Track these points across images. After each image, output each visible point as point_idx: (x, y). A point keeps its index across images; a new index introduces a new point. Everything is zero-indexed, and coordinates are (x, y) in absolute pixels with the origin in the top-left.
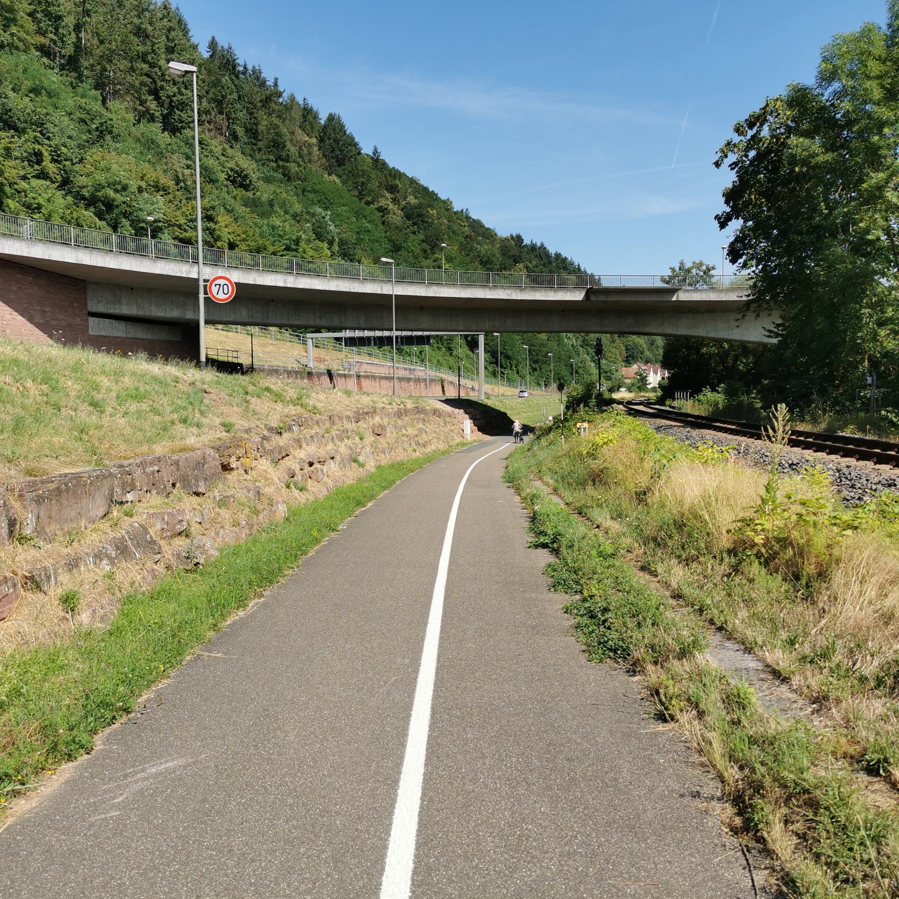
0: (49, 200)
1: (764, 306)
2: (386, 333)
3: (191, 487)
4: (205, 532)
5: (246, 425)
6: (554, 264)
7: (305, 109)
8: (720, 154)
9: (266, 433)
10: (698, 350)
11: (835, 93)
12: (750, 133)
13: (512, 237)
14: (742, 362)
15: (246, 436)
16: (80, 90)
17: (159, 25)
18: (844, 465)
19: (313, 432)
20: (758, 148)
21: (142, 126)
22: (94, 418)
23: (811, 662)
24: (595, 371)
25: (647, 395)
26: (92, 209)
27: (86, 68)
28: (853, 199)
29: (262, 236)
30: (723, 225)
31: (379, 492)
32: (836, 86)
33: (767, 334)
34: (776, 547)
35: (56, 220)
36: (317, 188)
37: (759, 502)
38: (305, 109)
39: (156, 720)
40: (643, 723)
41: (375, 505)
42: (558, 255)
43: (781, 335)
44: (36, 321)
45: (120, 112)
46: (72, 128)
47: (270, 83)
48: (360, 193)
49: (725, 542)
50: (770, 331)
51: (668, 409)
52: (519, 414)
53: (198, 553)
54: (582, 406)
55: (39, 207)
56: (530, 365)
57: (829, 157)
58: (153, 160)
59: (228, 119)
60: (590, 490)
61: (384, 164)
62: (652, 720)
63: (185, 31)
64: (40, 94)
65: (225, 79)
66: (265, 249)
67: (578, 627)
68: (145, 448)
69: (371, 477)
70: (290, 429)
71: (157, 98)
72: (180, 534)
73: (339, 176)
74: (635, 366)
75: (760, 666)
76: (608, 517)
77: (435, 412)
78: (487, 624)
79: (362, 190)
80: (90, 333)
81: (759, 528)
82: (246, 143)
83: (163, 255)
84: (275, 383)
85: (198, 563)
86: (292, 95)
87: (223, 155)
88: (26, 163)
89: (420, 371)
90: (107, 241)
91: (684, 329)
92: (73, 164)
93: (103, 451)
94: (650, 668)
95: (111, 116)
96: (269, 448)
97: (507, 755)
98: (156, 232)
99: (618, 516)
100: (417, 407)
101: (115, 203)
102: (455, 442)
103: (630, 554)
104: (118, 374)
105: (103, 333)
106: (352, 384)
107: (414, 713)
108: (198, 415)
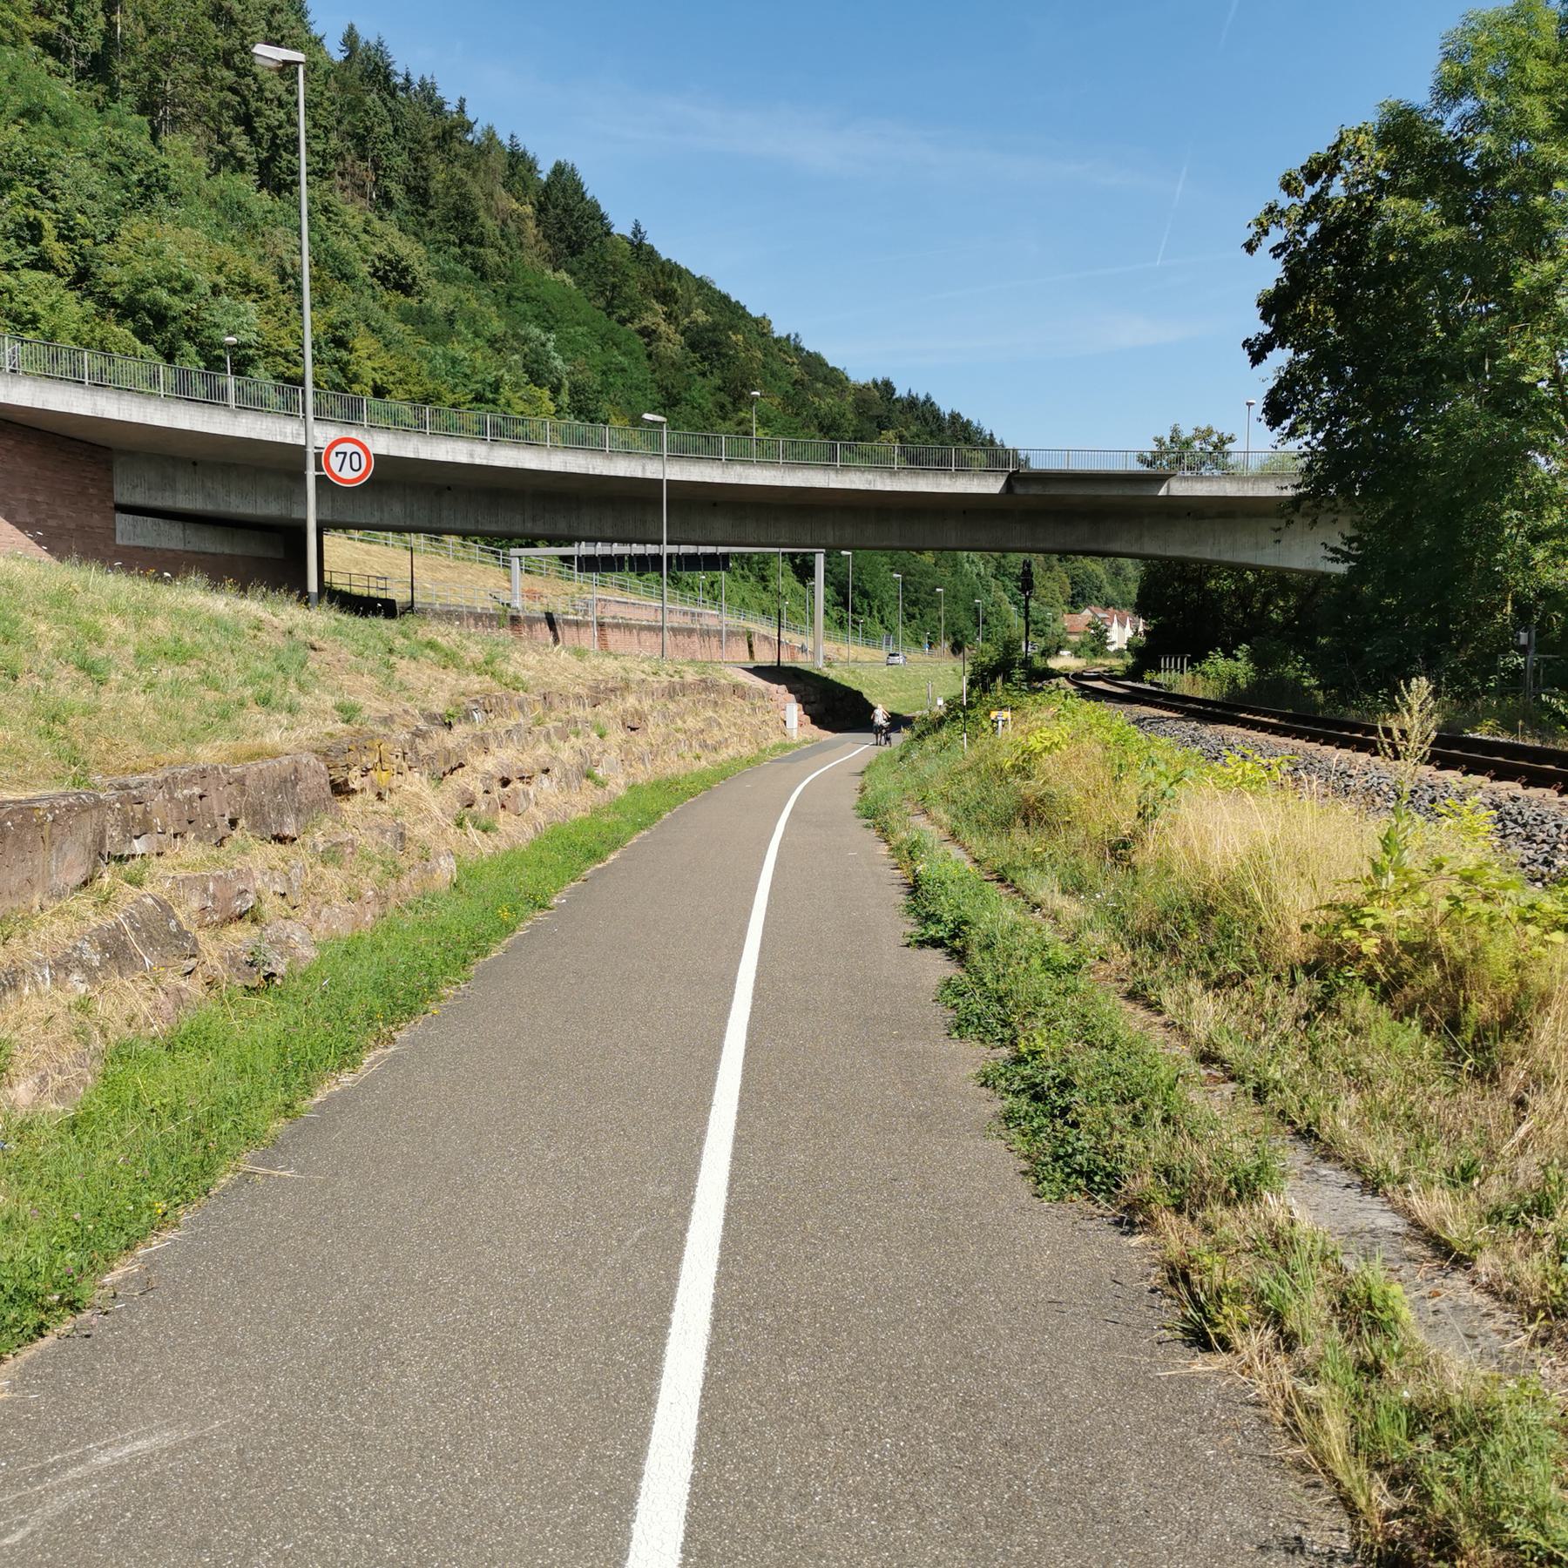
0: (52, 307)
1: (1326, 505)
2: (651, 549)
3: (268, 826)
4: (292, 913)
5: (386, 709)
6: (949, 432)
7: (512, 154)
8: (1254, 229)
9: (422, 724)
10: (1199, 582)
11: (1463, 118)
12: (1310, 191)
13: (875, 383)
14: (1277, 607)
15: (382, 730)
16: (112, 115)
18: (1503, 794)
19: (511, 723)
20: (1324, 219)
21: (221, 180)
22: (84, 692)
23: (1514, 1222)
24: (1017, 622)
25: (1107, 662)
27: (124, 77)
28: (1490, 313)
29: (433, 374)
30: (1257, 358)
31: (630, 836)
32: (1468, 105)
33: (1331, 555)
34: (1407, 962)
35: (65, 341)
36: (533, 292)
37: (1368, 870)
38: (512, 154)
39: (132, 1330)
40: (1159, 1352)
42: (955, 417)
43: (1354, 558)
44: (19, 519)
45: (182, 153)
46: (95, 181)
47: (451, 107)
48: (609, 304)
49: (1296, 948)
51: (1147, 686)
52: (882, 694)
53: (272, 956)
54: (999, 680)
55: (35, 319)
56: (904, 609)
57: (1452, 234)
58: (238, 238)
59: (376, 170)
60: (1018, 833)
61: (652, 252)
62: (1180, 1346)
64: (39, 119)
65: (371, 99)
66: (439, 399)
67: (1009, 1117)
68: (178, 752)
69: (617, 805)
70: (468, 717)
71: (250, 131)
72: (240, 917)
73: (572, 273)
74: (1087, 612)
75: (1401, 1226)
76: (1056, 889)
77: (736, 689)
78: (829, 1108)
79: (613, 298)
80: (119, 541)
81: (1369, 922)
83: (252, 404)
84: (445, 635)
85: (273, 975)
86: (490, 128)
87: (366, 231)
88: (12, 241)
89: (711, 617)
90: (153, 380)
91: (1176, 546)
92: (96, 244)
93: (91, 756)
94: (1167, 1219)
95: (164, 159)
97: (873, 1428)
98: (241, 366)
99: (1076, 887)
102: (771, 743)
103: (1103, 965)
104: (144, 612)
105: (141, 542)
106: (589, 638)
107: (676, 1317)
108: (294, 690)
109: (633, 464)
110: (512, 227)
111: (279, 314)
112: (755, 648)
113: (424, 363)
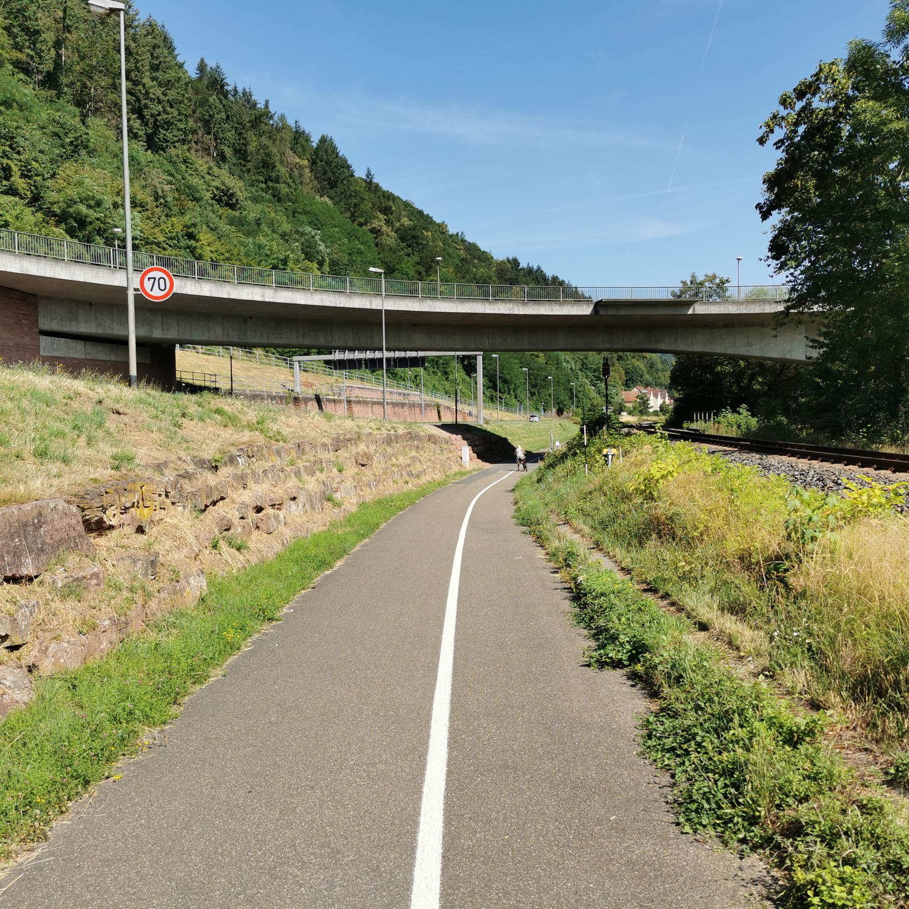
0: (17, 217)
2: (378, 355)
7: (297, 132)
8: (764, 129)
9: (191, 468)
12: (799, 105)
13: (508, 260)
17: (143, 41)
19: (267, 465)
25: (649, 418)
26: (63, 226)
29: (247, 255)
30: (765, 216)
31: (354, 544)
36: (308, 209)
38: (297, 132)
41: (346, 564)
43: (826, 345)
46: (44, 143)
47: (261, 105)
48: (353, 215)
50: (813, 341)
52: (519, 440)
54: (605, 428)
61: (377, 186)
63: (171, 48)
64: (11, 106)
65: (213, 99)
69: (349, 520)
70: (232, 460)
73: (331, 198)
74: (635, 390)
77: (430, 438)
79: (355, 212)
82: (234, 165)
87: (209, 174)
89: (415, 396)
91: (698, 345)
92: (44, 180)
96: (190, 489)
100: (410, 433)
101: (88, 220)
106: (342, 409)
109: (364, 300)
110: (296, 172)
111: (154, 220)
112: (442, 414)
113: (242, 248)
